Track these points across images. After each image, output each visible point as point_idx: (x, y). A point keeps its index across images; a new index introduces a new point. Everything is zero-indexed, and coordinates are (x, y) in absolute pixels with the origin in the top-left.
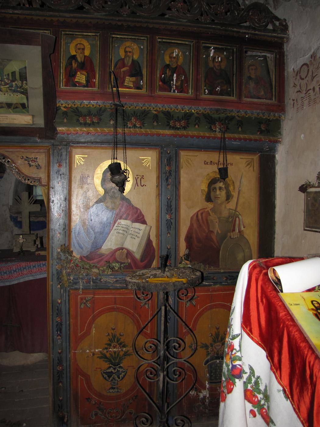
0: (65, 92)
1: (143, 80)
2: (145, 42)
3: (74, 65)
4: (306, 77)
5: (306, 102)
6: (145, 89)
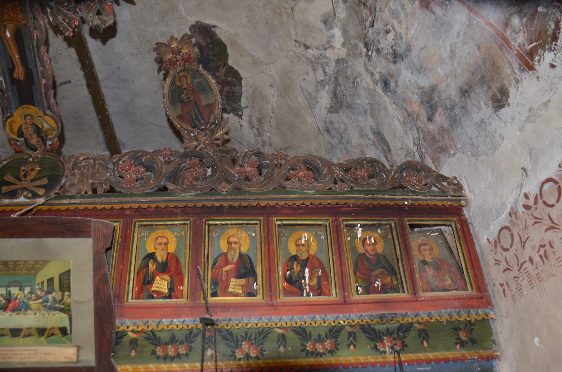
0: (134, 308)
1: (258, 281)
2: (257, 227)
3: (152, 267)
4: (511, 247)
5: (525, 283)
6: (261, 296)
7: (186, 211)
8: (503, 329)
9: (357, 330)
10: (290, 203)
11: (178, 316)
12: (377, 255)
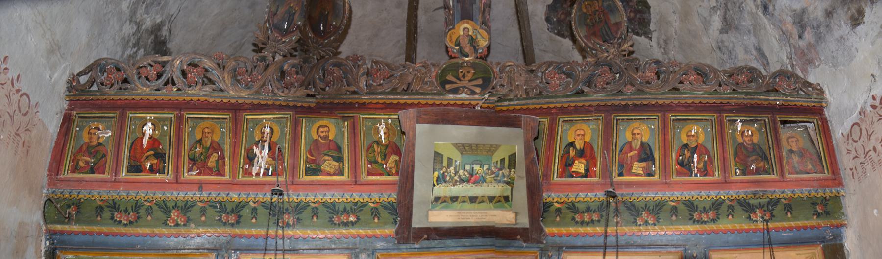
3: (572, 153)
5: (869, 167)
7: (599, 109)
8: (851, 205)
9: (735, 204)
10: (683, 102)
11: (592, 191)
12: (753, 144)
